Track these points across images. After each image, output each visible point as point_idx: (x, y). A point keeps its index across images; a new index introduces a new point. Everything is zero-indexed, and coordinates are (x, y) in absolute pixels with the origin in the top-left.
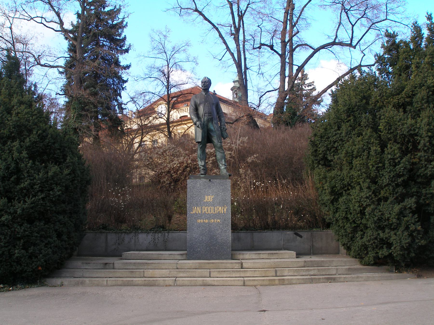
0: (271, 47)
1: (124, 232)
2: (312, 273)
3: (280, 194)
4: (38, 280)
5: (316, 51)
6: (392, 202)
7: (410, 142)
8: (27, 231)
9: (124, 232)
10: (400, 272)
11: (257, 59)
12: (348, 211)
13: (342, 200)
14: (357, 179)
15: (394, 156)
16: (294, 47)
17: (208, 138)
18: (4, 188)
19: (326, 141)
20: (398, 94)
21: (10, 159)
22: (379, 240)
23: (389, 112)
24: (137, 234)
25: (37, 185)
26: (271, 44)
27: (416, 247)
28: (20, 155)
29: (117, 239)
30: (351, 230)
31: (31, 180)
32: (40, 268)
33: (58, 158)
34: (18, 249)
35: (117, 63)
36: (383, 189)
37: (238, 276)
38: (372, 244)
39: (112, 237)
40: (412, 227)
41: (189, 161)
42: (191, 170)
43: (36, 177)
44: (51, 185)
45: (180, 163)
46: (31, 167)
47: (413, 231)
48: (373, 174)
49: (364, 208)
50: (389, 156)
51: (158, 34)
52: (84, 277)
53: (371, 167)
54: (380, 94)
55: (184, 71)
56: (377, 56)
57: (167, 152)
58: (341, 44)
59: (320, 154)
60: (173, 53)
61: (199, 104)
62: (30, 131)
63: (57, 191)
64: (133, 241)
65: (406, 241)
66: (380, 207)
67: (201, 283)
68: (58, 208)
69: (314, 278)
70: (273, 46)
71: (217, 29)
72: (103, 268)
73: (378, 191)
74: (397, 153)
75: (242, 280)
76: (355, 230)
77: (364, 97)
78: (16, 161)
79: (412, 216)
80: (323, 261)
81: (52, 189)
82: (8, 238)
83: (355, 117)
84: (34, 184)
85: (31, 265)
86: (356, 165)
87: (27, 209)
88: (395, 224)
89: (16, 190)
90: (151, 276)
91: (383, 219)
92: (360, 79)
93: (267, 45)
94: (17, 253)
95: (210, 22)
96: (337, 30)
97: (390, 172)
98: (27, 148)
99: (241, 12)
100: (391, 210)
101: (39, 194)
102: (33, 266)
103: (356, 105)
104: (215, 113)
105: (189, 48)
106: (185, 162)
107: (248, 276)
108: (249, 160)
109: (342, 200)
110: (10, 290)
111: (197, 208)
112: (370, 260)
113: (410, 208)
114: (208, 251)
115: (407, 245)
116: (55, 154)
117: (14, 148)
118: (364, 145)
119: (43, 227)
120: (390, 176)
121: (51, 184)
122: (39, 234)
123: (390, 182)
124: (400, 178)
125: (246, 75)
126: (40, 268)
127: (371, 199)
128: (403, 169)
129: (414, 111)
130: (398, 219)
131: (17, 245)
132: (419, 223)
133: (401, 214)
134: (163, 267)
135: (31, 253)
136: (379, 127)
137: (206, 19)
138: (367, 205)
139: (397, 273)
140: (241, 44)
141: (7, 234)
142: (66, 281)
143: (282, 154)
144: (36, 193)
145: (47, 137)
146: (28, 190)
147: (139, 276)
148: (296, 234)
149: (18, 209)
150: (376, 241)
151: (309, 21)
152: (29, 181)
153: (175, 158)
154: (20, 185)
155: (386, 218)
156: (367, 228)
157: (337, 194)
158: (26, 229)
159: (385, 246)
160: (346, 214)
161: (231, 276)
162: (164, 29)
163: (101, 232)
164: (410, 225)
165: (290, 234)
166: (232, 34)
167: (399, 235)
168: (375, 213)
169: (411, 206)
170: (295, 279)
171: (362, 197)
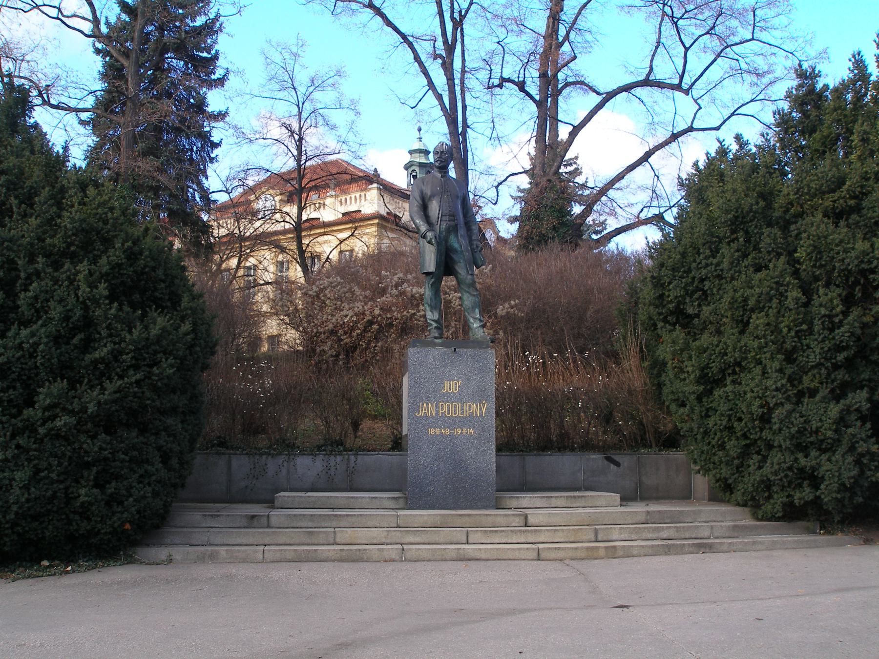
0: (521, 86)
1: (266, 453)
2: (665, 534)
3: (576, 382)
4: (120, 550)
5: (610, 96)
6: (824, 398)
7: (859, 283)
8: (105, 450)
9: (266, 453)
10: (828, 533)
11: (488, 107)
12: (734, 415)
13: (721, 393)
14: (756, 355)
15: (831, 311)
16: (560, 86)
17: (446, 266)
18: (59, 360)
19: (683, 278)
20: (833, 191)
21: (72, 300)
22: (796, 471)
23: (816, 224)
24: (292, 457)
25: (127, 354)
26: (521, 79)
27: (866, 484)
28: (92, 290)
29: (252, 467)
30: (739, 451)
31: (115, 343)
32: (128, 526)
33: (161, 299)
34: (85, 487)
35: (200, 106)
36: (806, 373)
37: (523, 540)
38: (781, 480)
39: (241, 464)
40: (862, 447)
41: (377, 311)
42: (408, 330)
43: (125, 337)
44: (154, 355)
45: (356, 315)
46: (116, 316)
47: (862, 455)
48: (788, 346)
49: (771, 410)
50: (823, 311)
51: (280, 49)
52: (210, 545)
53: (785, 330)
54: (798, 190)
55: (333, 127)
56: (779, 114)
57: (327, 292)
58: (660, 85)
59: (671, 302)
60: (311, 89)
61: (431, 197)
62: (107, 242)
63: (167, 367)
64: (284, 471)
65: (850, 473)
66: (803, 409)
67: (454, 555)
68: (164, 401)
69: (673, 545)
70: (524, 82)
71: (411, 45)
72: (246, 525)
73: (798, 377)
74: (838, 306)
75: (534, 549)
76: (745, 453)
77: (762, 195)
78: (84, 303)
79: (862, 426)
80: (681, 513)
81: (156, 363)
82: (66, 463)
83: (747, 232)
84: (121, 353)
85: (110, 519)
86: (758, 326)
87: (107, 404)
88: (829, 441)
89: (83, 364)
90: (349, 542)
91: (806, 430)
92: (736, 158)
93: (513, 82)
94: (84, 493)
95: (396, 29)
96: (653, 55)
97: (823, 341)
98: (104, 276)
99: (460, 12)
100: (823, 413)
101: (131, 372)
102: (114, 522)
103: (751, 210)
104: (461, 216)
105: (342, 81)
106: (368, 313)
107: (541, 541)
108: (501, 310)
109: (721, 393)
110: (67, 572)
111: (428, 404)
112: (775, 510)
113: (858, 410)
114: (455, 491)
115: (852, 481)
116: (156, 289)
117: (81, 277)
118: (772, 289)
119: (136, 440)
120: (822, 348)
121: (156, 352)
122: (126, 455)
123: (822, 360)
124: (840, 352)
125: (465, 140)
126: (128, 526)
127: (785, 392)
128: (849, 337)
129: (866, 225)
130: (836, 431)
131: (82, 477)
132: (873, 440)
133: (842, 421)
134: (370, 524)
135: (111, 495)
136: (796, 255)
137: (389, 23)
138: (776, 404)
139: (824, 534)
140: (457, 76)
141: (64, 454)
142: (178, 553)
143: (564, 301)
144: (123, 370)
145: (141, 255)
146: (107, 365)
147: (325, 542)
148: (609, 459)
149: (89, 402)
150: (790, 474)
151: (598, 37)
152: (110, 346)
153: (346, 305)
154: (90, 353)
155: (814, 429)
156: (770, 446)
157: (711, 383)
158: (104, 446)
159: (806, 483)
160: (730, 420)
161: (509, 541)
162: (294, 41)
163: (218, 453)
164: (858, 442)
165: (596, 459)
166: (436, 56)
167: (837, 461)
168: (793, 419)
169: (860, 406)
170: (637, 546)
171: (766, 388)
